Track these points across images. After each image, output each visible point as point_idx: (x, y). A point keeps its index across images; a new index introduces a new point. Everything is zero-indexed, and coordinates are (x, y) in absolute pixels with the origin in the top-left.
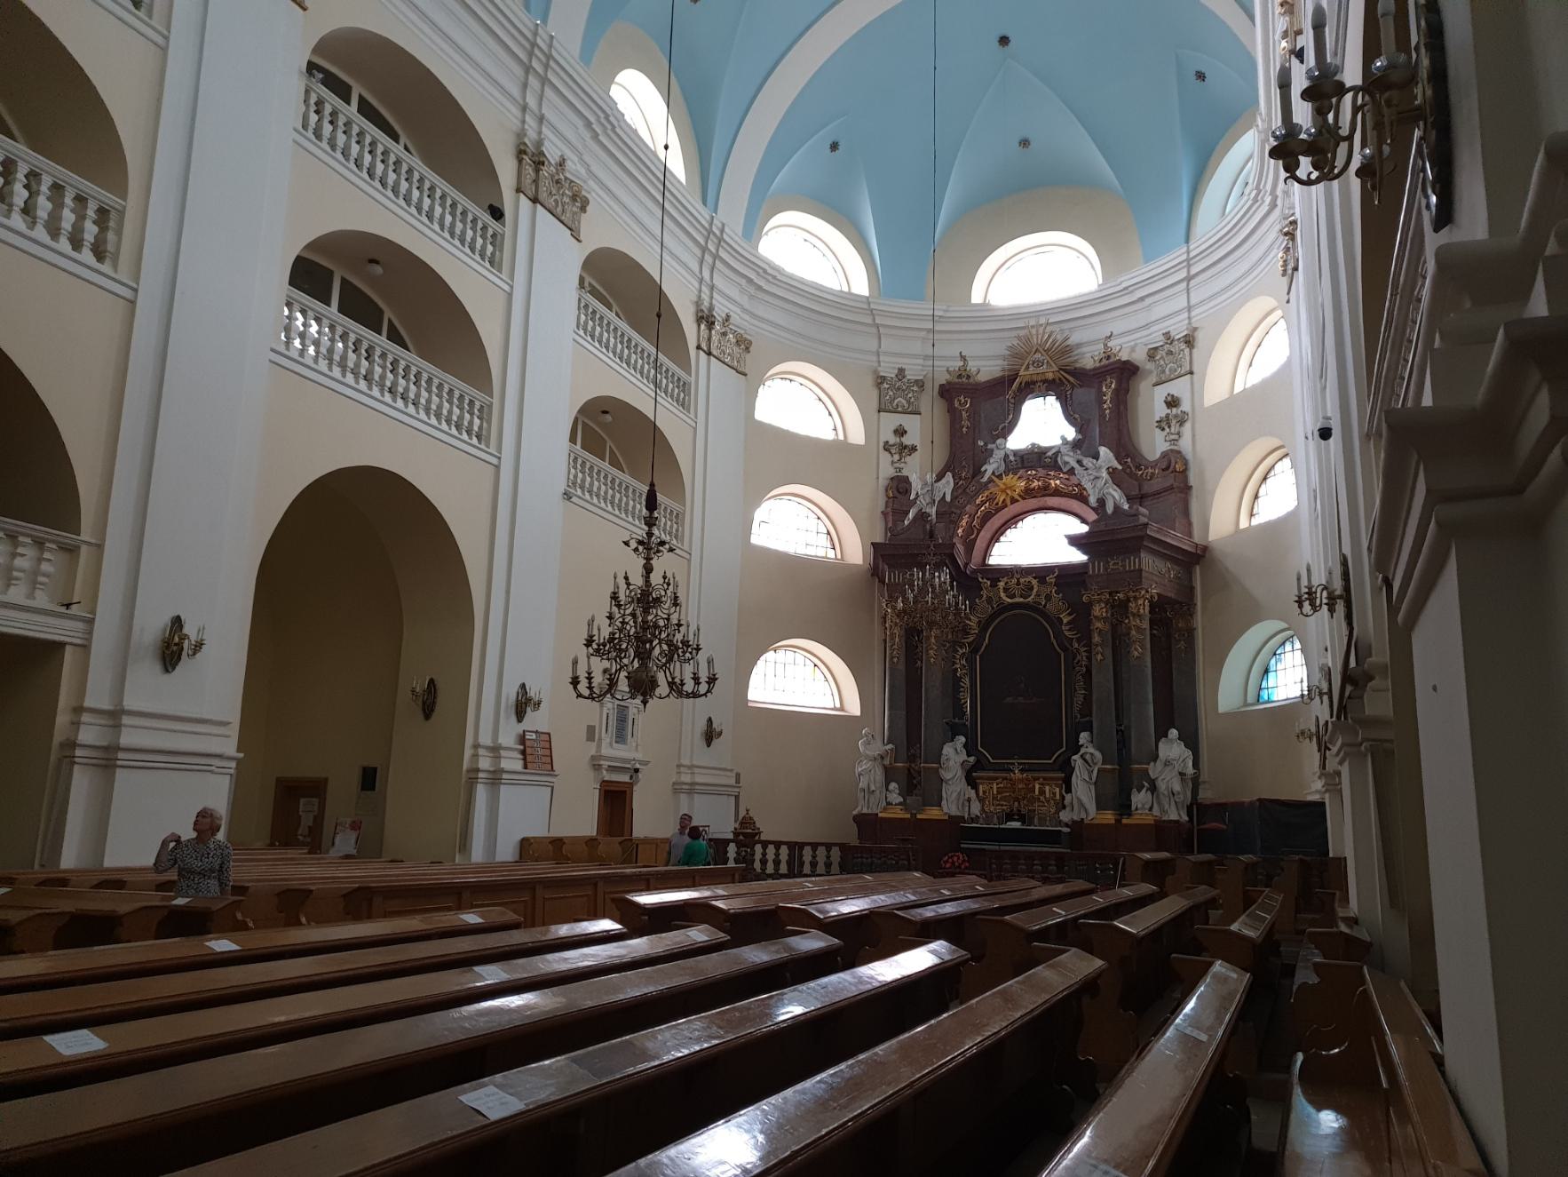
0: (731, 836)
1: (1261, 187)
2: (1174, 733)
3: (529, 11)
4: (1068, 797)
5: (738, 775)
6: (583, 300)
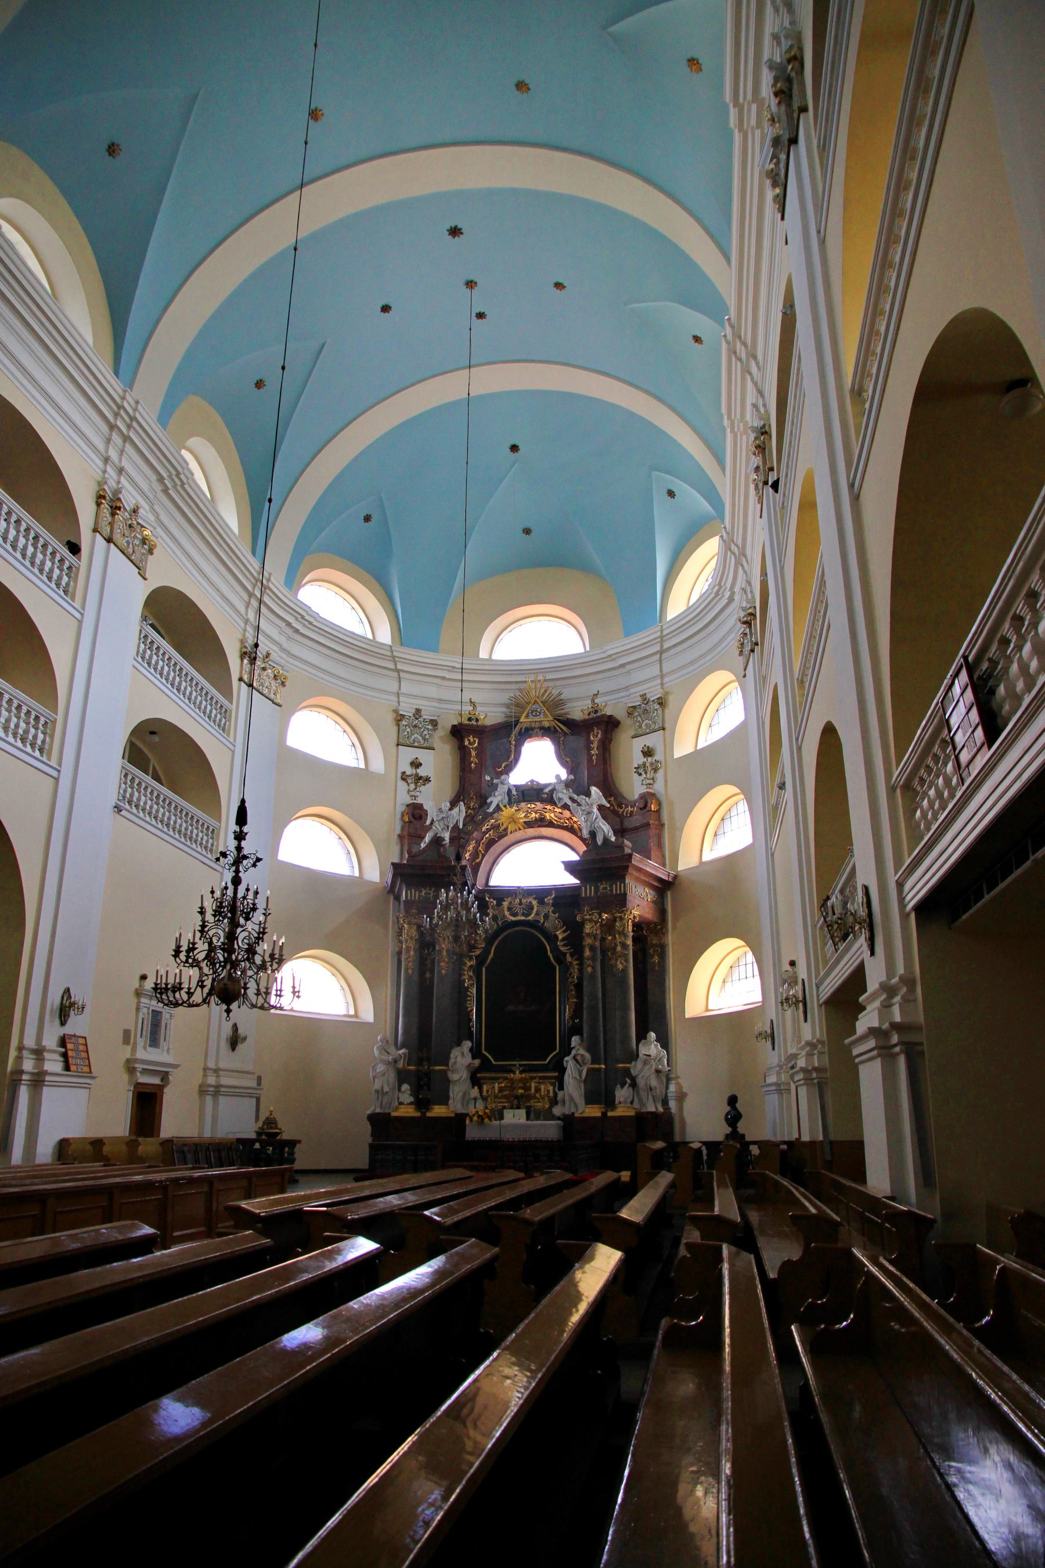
0: (253, 1136)
1: (722, 584)
2: (653, 1035)
3: (118, 378)
4: (560, 1094)
5: (259, 1079)
6: (143, 631)
